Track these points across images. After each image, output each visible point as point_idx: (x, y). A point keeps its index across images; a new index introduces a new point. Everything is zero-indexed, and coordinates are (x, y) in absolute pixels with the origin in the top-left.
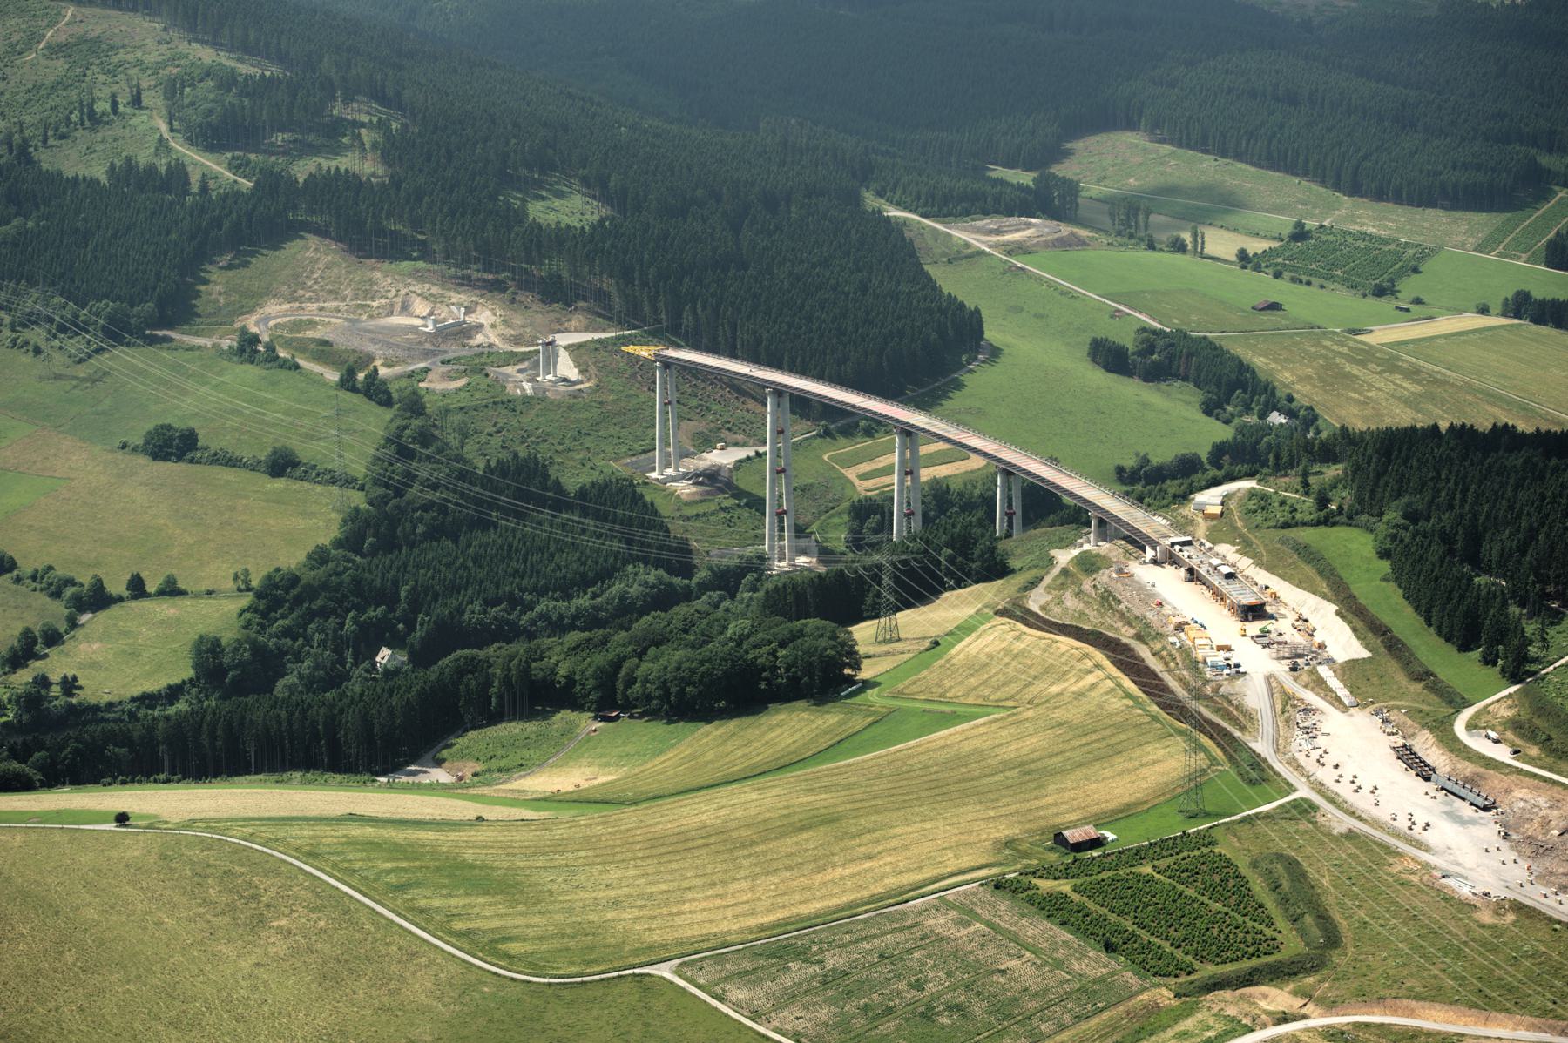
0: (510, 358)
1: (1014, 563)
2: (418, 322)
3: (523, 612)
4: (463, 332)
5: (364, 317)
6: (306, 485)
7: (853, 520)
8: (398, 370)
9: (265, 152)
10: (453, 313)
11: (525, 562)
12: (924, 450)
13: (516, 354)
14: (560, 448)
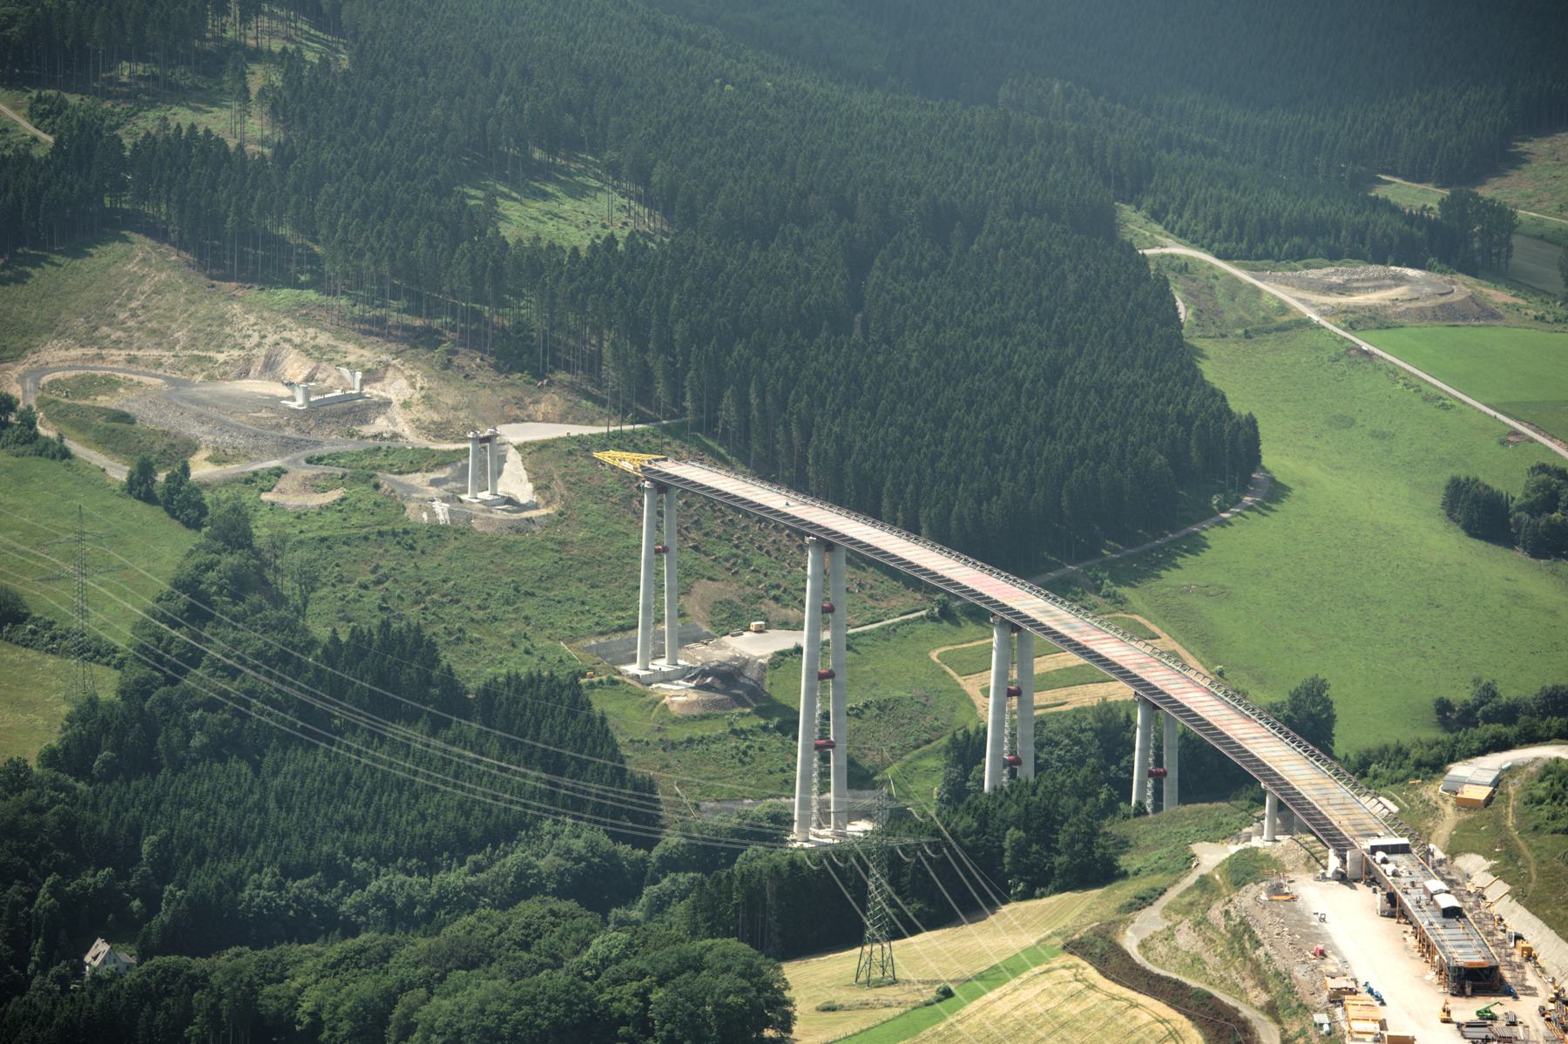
0: (422, 460)
1: (1124, 861)
2: (282, 391)
3: (347, 891)
4: (354, 411)
5: (199, 378)
6: (32, 654)
7: (954, 764)
8: (232, 469)
9: (95, 92)
10: (343, 381)
11: (367, 805)
12: (1042, 665)
13: (433, 453)
14: (480, 614)
